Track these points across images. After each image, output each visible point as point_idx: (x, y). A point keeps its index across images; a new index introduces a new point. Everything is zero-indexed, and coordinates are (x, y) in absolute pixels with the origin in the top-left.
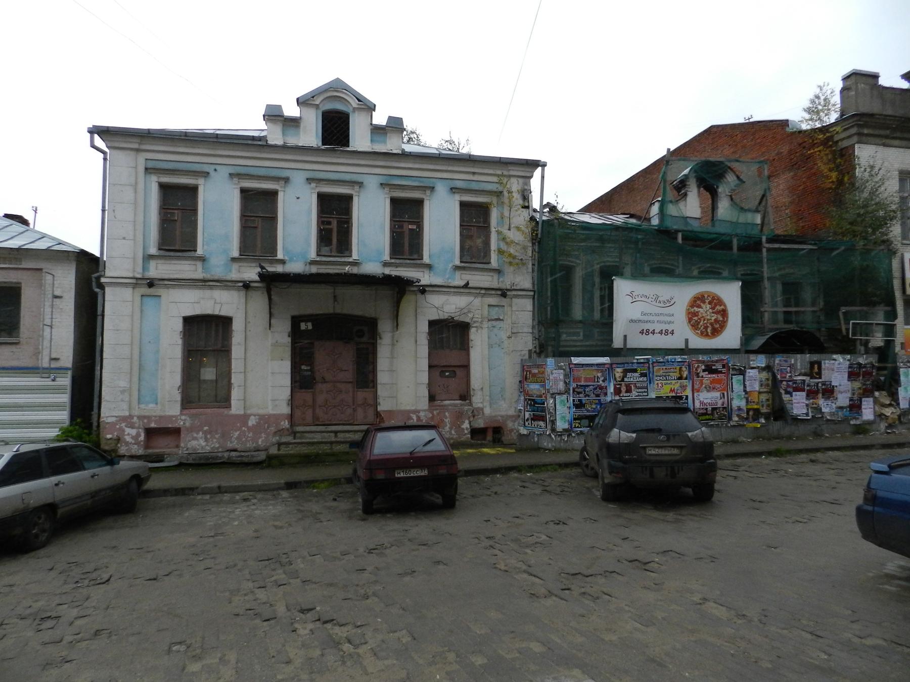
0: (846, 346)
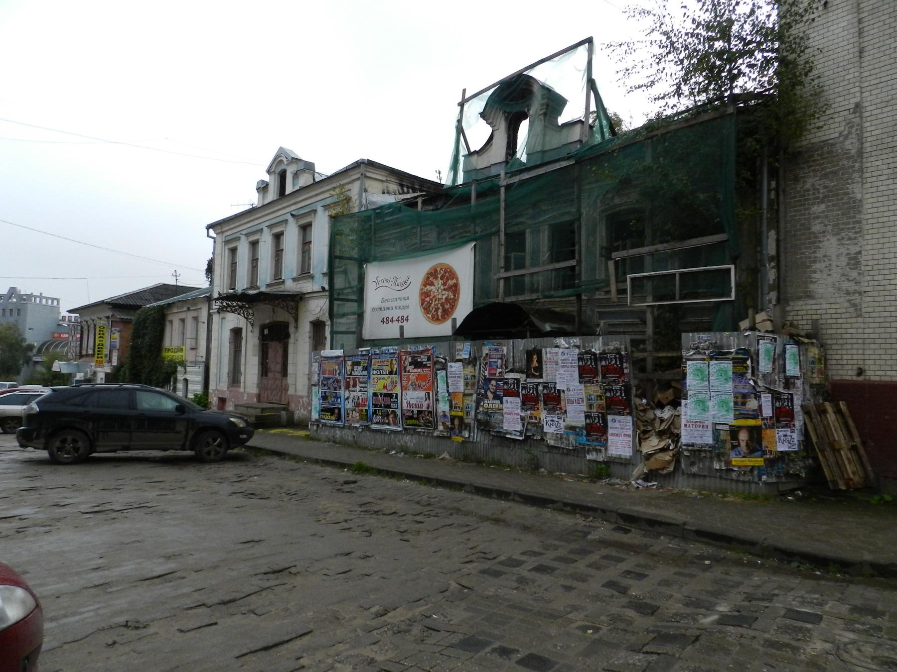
0: (574, 325)
